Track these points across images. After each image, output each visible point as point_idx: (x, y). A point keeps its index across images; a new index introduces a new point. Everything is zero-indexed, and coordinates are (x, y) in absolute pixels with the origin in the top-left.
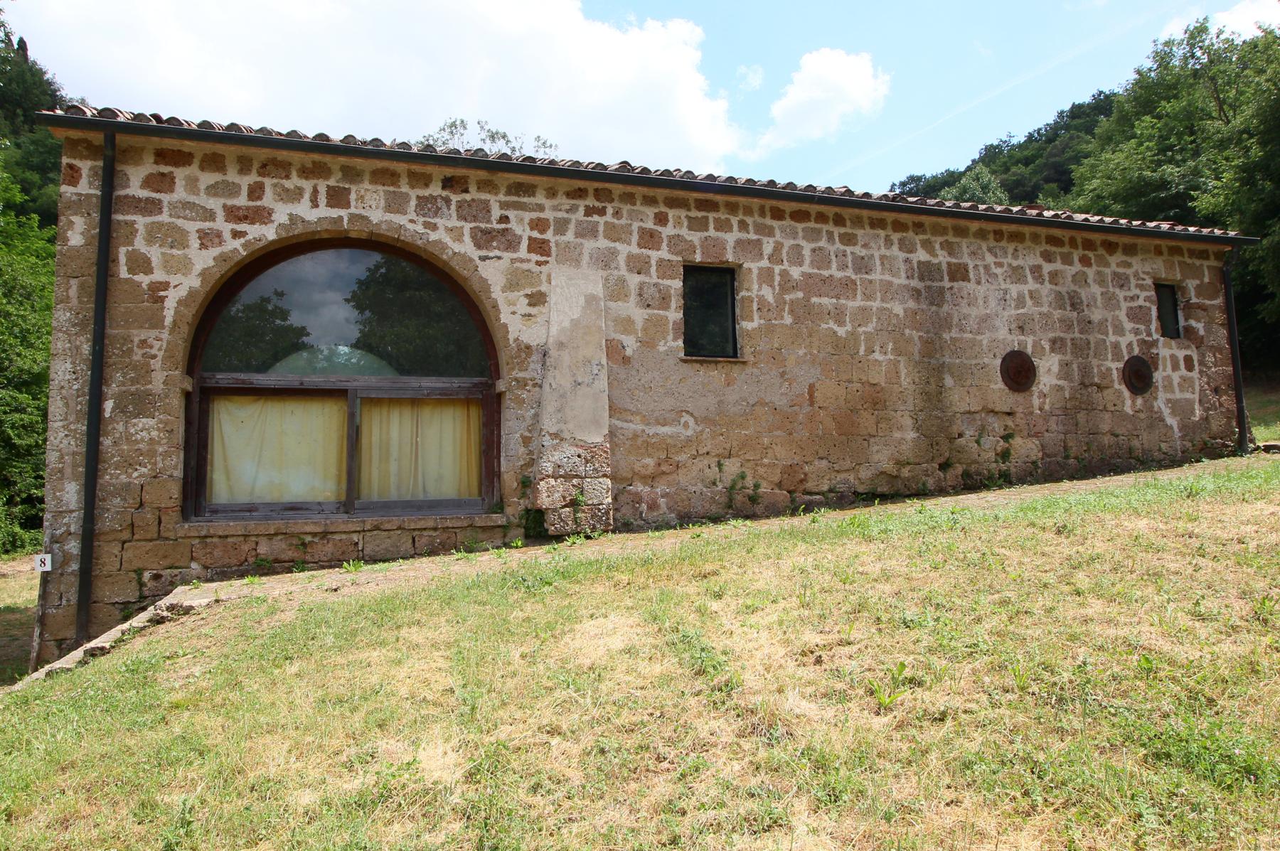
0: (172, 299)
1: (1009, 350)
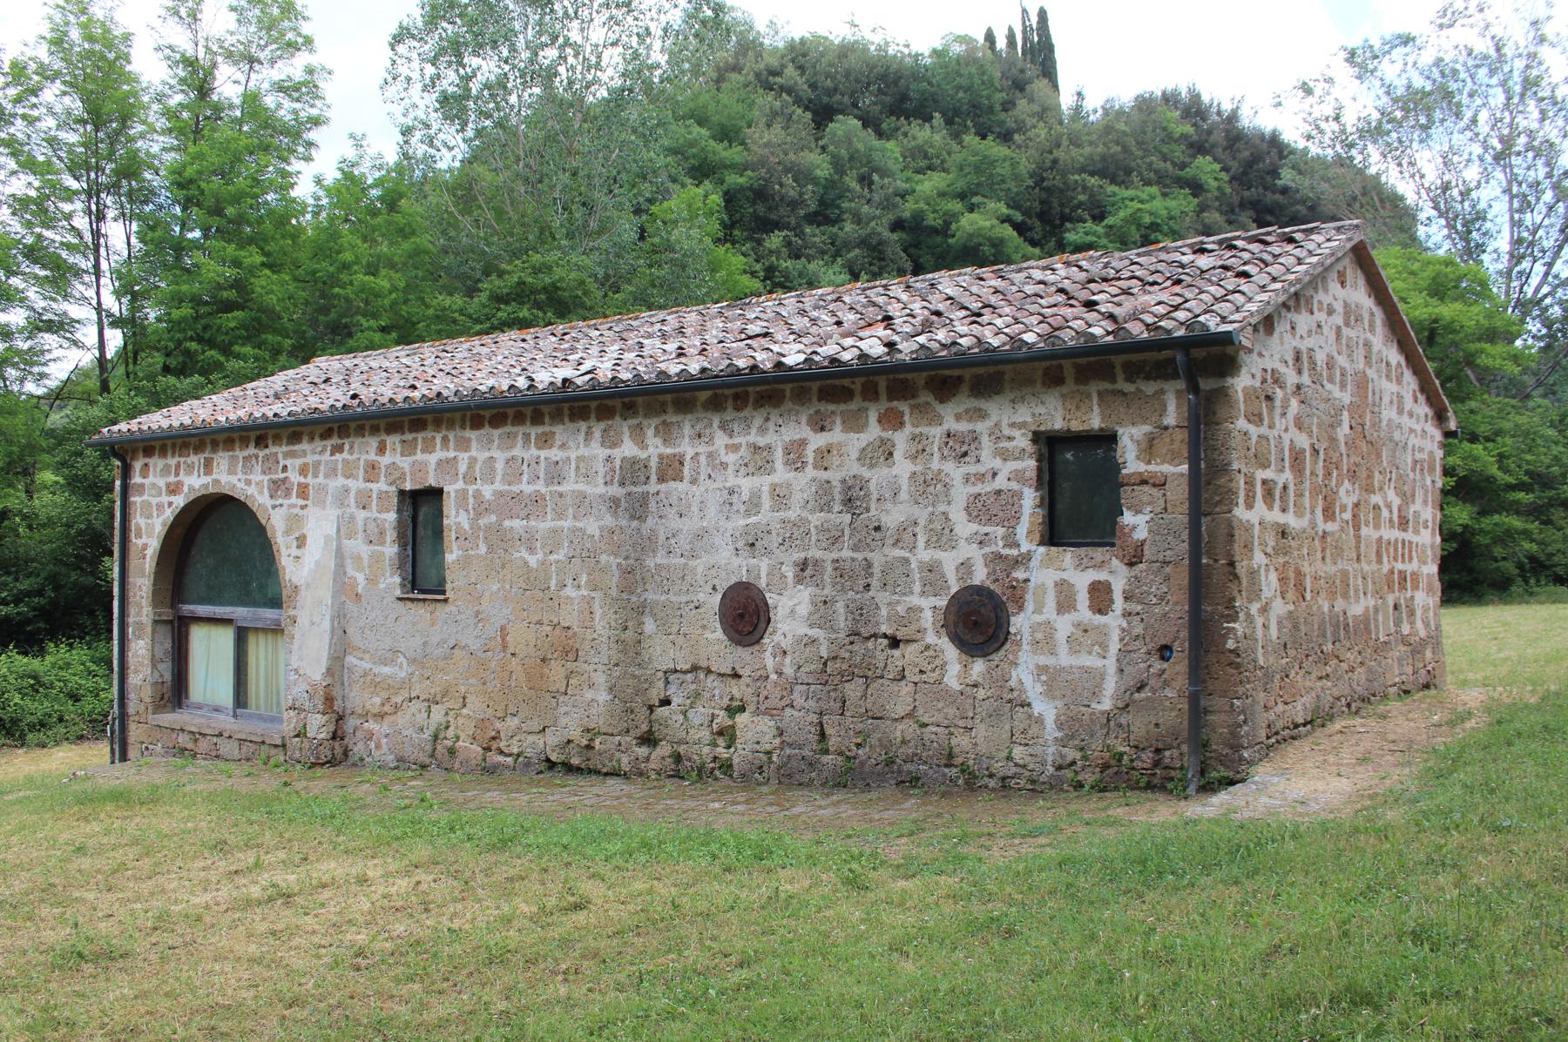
1: (733, 580)
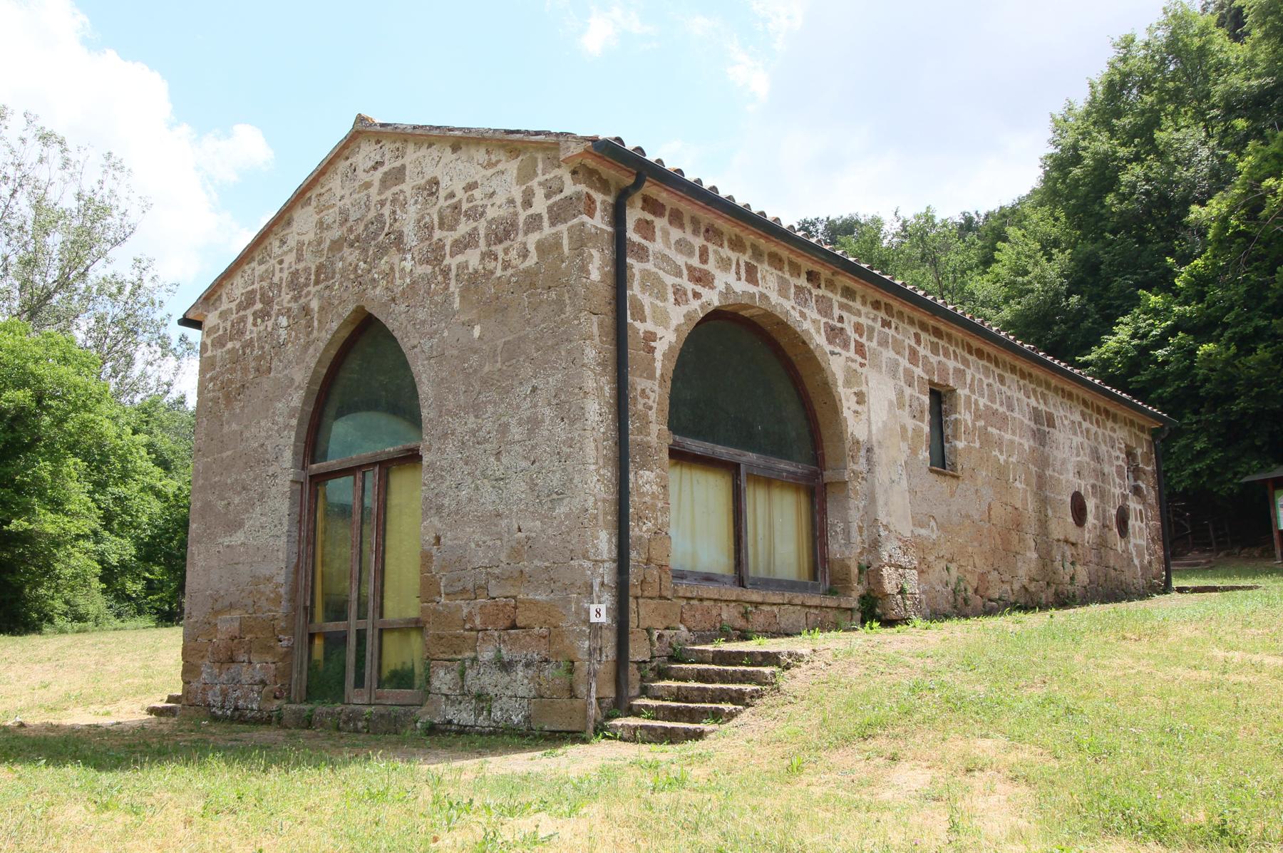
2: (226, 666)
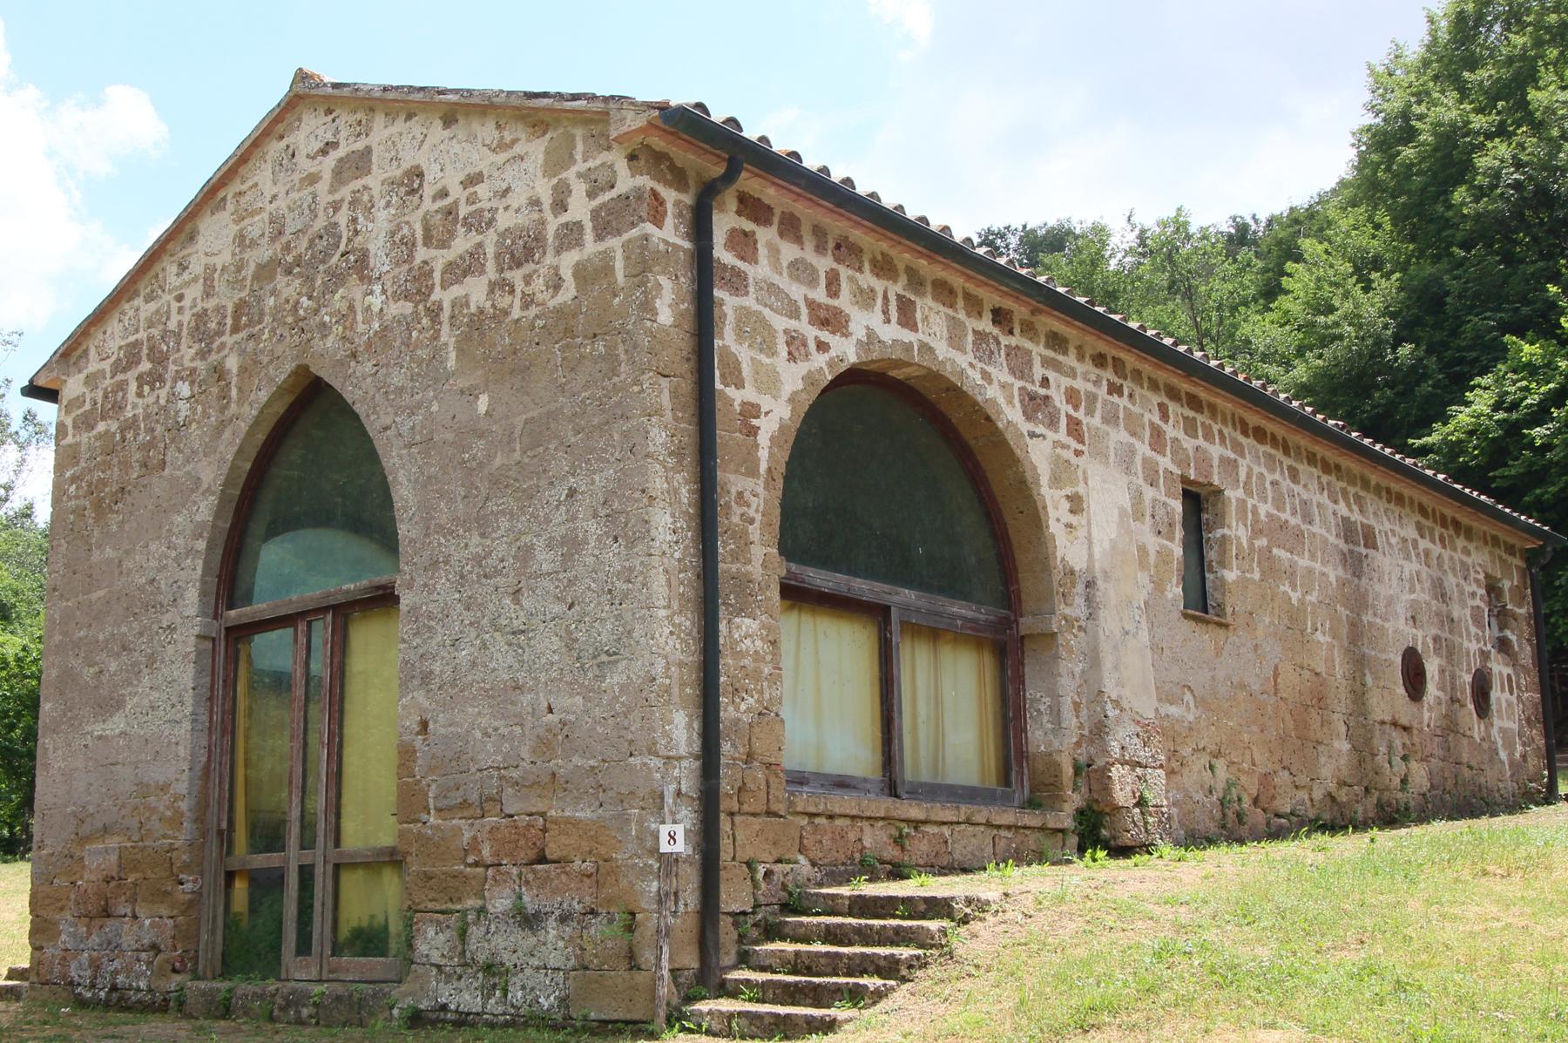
0: (767, 427)
2: (98, 922)
